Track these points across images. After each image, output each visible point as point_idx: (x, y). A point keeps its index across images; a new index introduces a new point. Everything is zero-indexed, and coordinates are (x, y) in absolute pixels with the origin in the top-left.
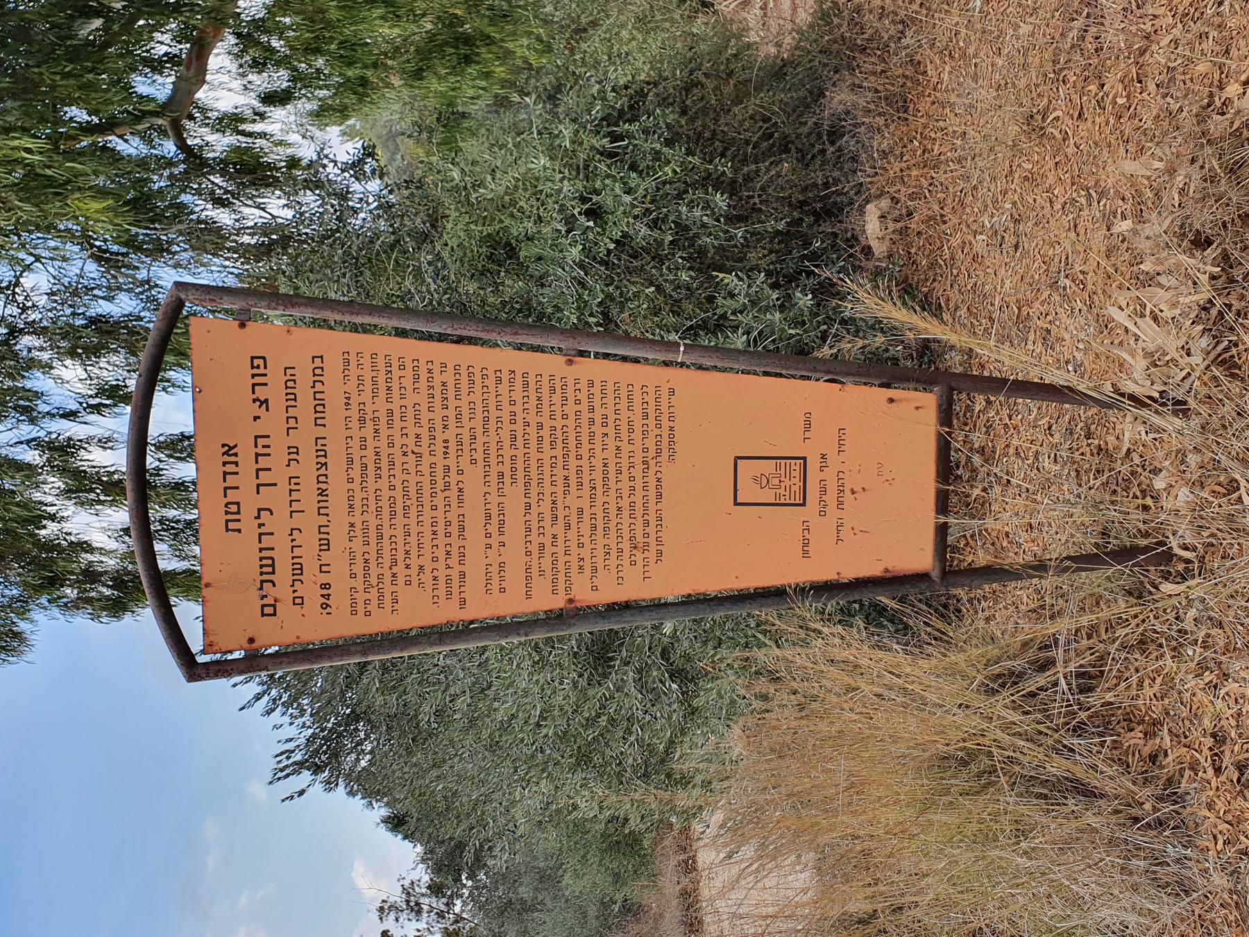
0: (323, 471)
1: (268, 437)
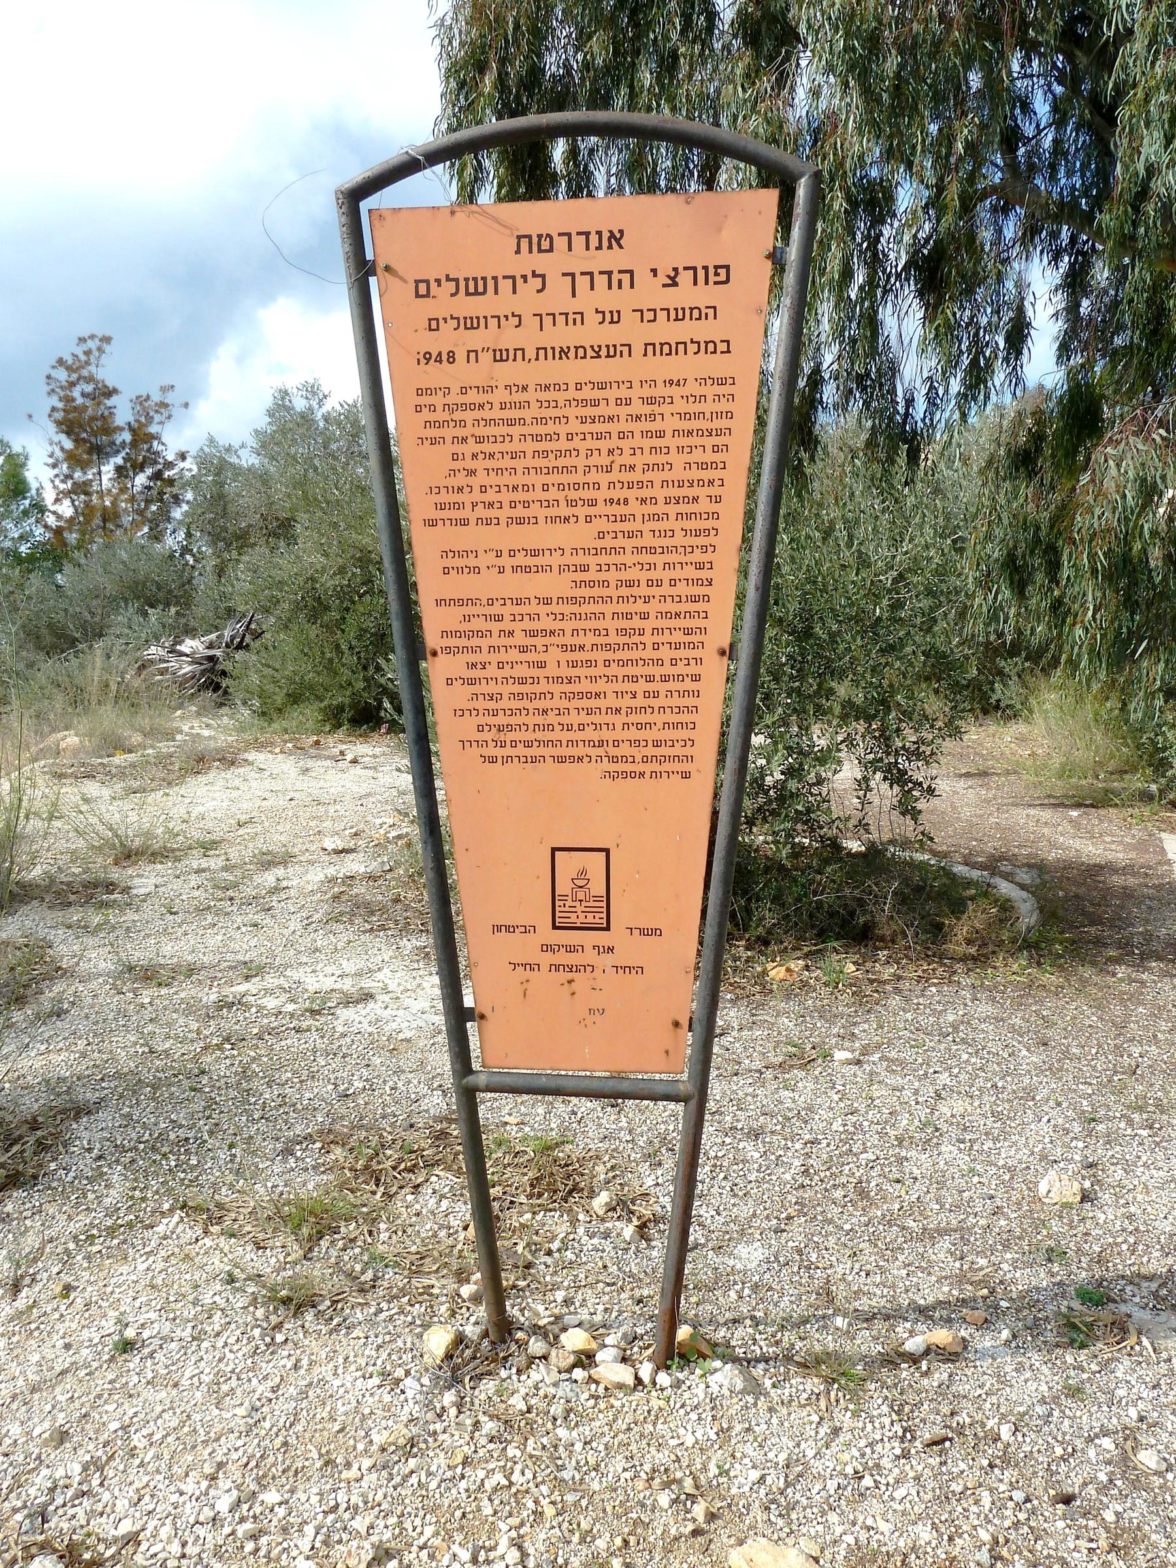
0: (590, 353)
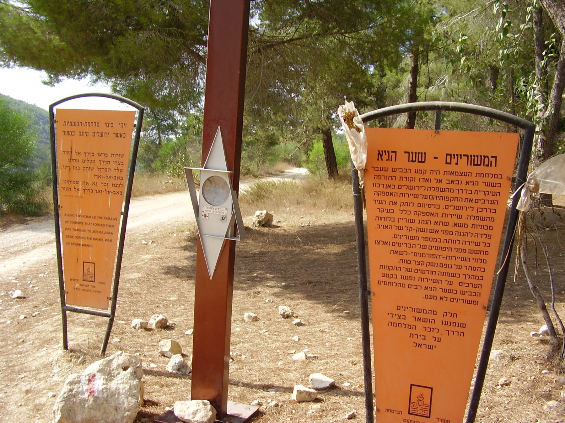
0: (459, 174)
1: (496, 166)
